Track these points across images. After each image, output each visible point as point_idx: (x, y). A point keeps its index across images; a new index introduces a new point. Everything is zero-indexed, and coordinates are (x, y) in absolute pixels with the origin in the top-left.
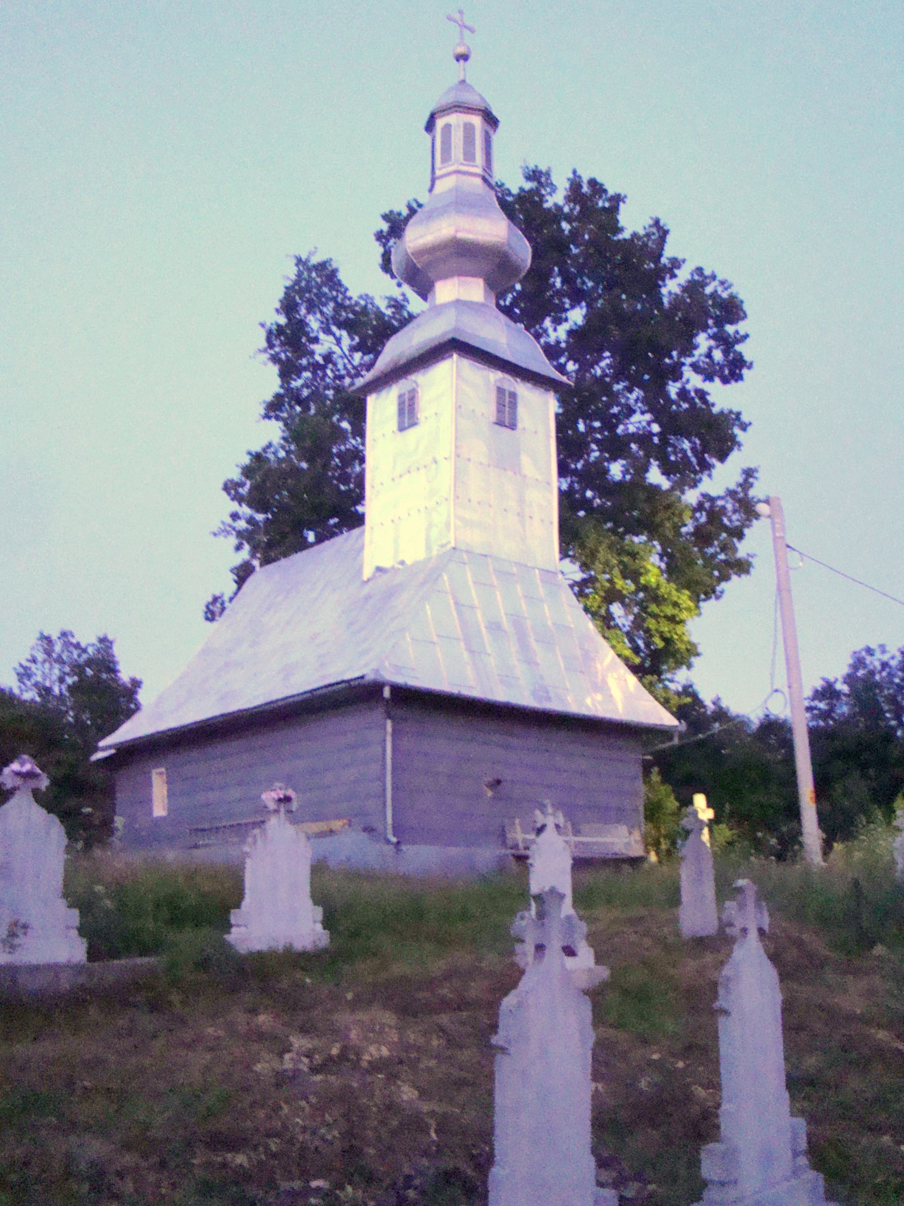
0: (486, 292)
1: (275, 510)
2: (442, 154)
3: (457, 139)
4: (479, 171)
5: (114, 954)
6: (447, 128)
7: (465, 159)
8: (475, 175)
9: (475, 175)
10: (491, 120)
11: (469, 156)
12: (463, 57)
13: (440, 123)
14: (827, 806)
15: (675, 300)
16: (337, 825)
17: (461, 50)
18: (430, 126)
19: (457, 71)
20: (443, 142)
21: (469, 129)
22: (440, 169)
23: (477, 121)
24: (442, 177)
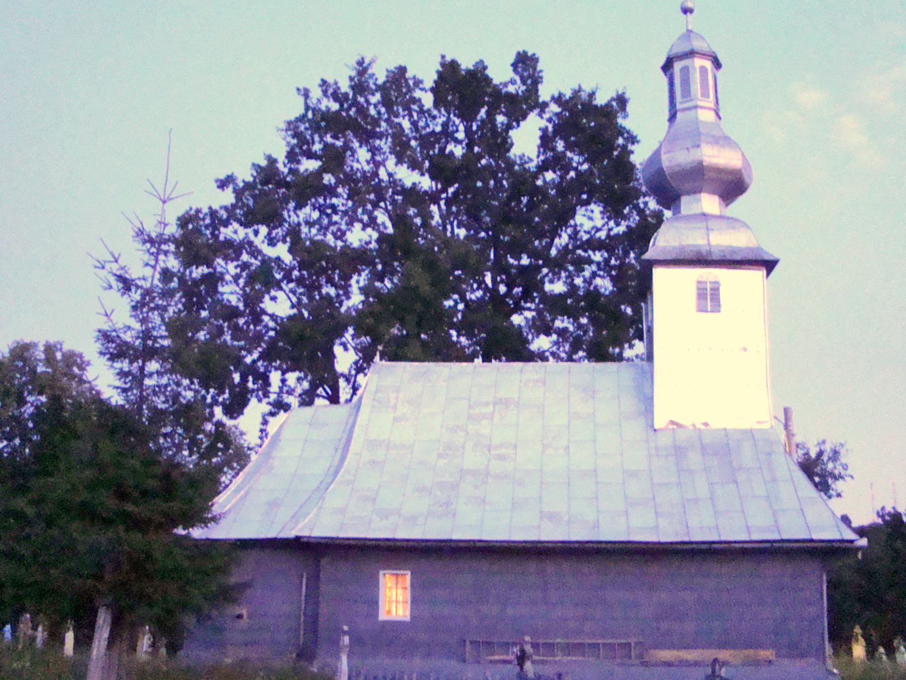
0: (720, 204)
1: (342, 176)
2: (682, 91)
3: (696, 77)
4: (712, 105)
5: (594, 644)
6: (685, 71)
7: (702, 96)
8: (710, 109)
9: (710, 109)
10: (717, 64)
11: (705, 95)
12: (686, 11)
13: (678, 66)
14: (647, 390)
15: (728, 199)
16: (767, 654)
17: (689, 5)
18: (667, 67)
19: (680, 23)
20: (707, 80)
21: (703, 70)
22: (681, 103)
23: (708, 64)
24: (683, 110)
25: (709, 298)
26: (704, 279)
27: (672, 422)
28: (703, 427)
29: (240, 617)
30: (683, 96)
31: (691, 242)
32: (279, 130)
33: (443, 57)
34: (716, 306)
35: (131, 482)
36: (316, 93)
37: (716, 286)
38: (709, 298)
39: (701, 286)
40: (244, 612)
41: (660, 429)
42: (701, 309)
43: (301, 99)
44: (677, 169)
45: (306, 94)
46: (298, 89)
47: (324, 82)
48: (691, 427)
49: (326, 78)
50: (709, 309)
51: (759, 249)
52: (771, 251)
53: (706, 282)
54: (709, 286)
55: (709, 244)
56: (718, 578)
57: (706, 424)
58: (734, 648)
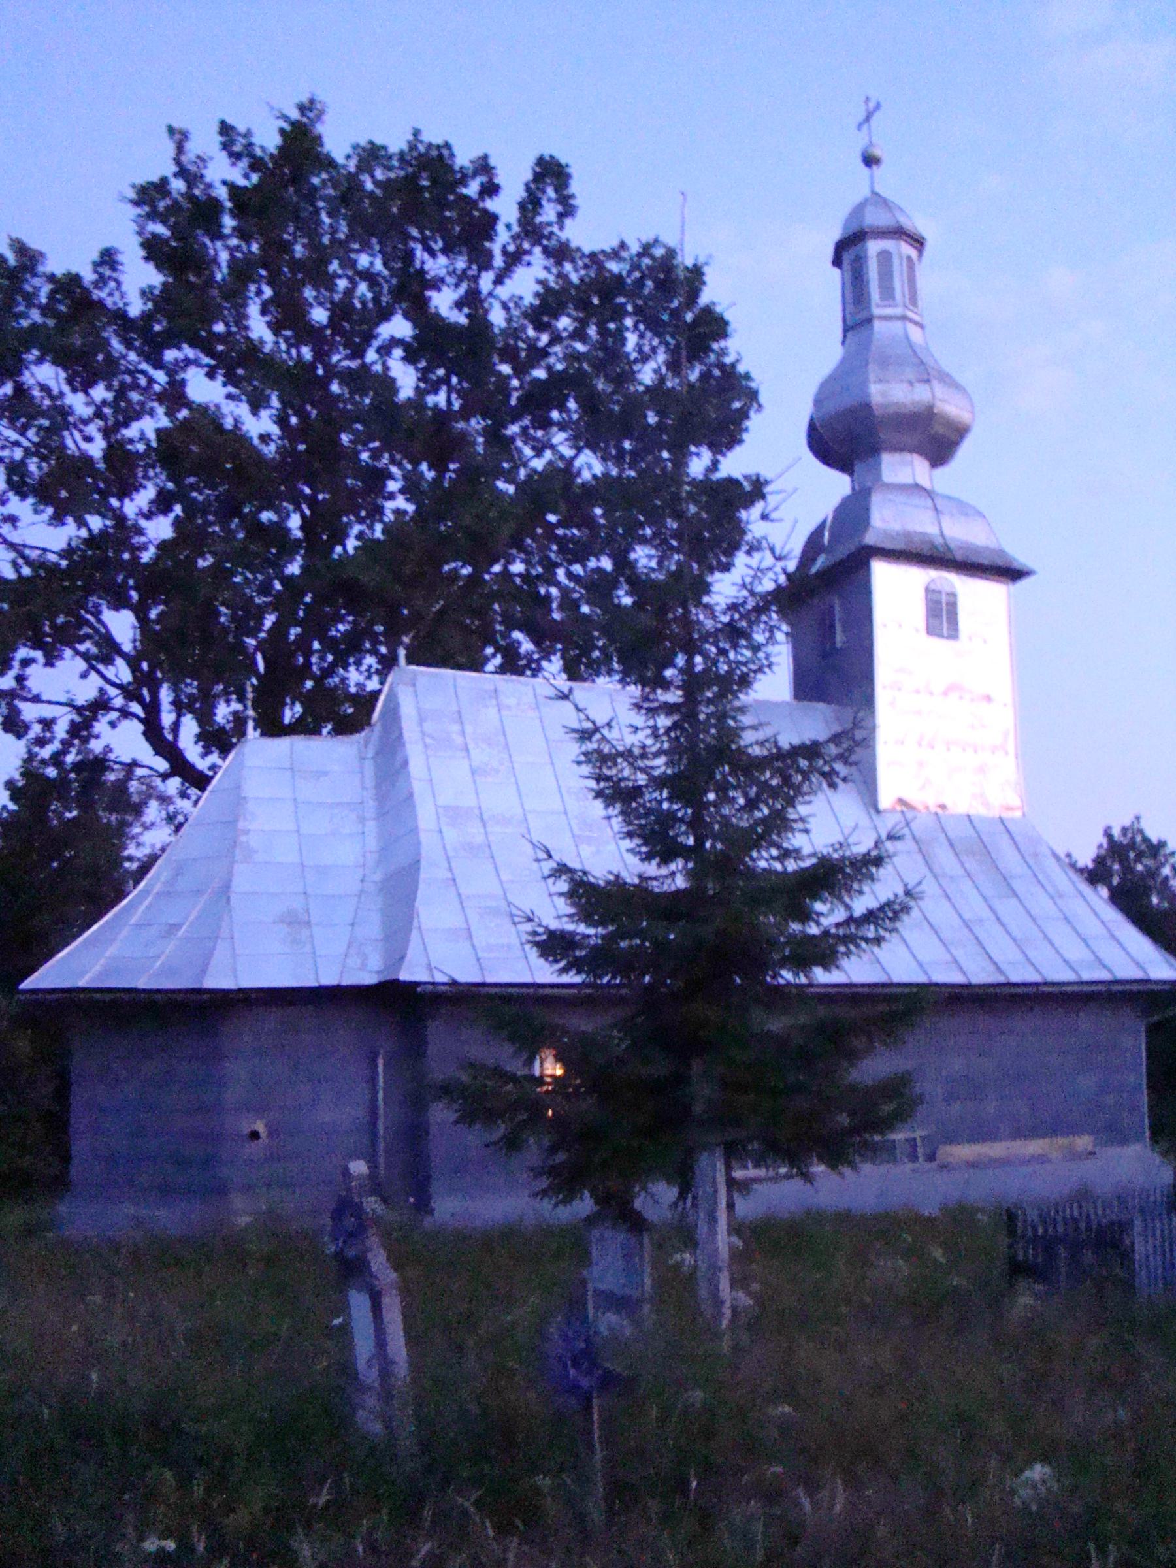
16: (1084, 1142)
17: (877, 152)
22: (878, 306)
25: (942, 617)
26: (938, 587)
27: (901, 801)
28: (940, 811)
29: (255, 1135)
30: (882, 298)
31: (919, 528)
32: (123, 199)
33: (416, 133)
34: (953, 633)
35: (378, 877)
36: (205, 143)
37: (951, 599)
38: (942, 617)
39: (935, 597)
40: (260, 1127)
41: (885, 811)
42: (931, 631)
43: (170, 148)
44: (891, 410)
45: (180, 137)
46: (867, 99)
47: (225, 129)
48: (924, 811)
49: (230, 121)
50: (945, 632)
51: (1001, 553)
52: (1020, 556)
53: (940, 592)
54: (944, 599)
55: (942, 535)
56: (1023, 1034)
57: (943, 807)
58: (1043, 1136)
